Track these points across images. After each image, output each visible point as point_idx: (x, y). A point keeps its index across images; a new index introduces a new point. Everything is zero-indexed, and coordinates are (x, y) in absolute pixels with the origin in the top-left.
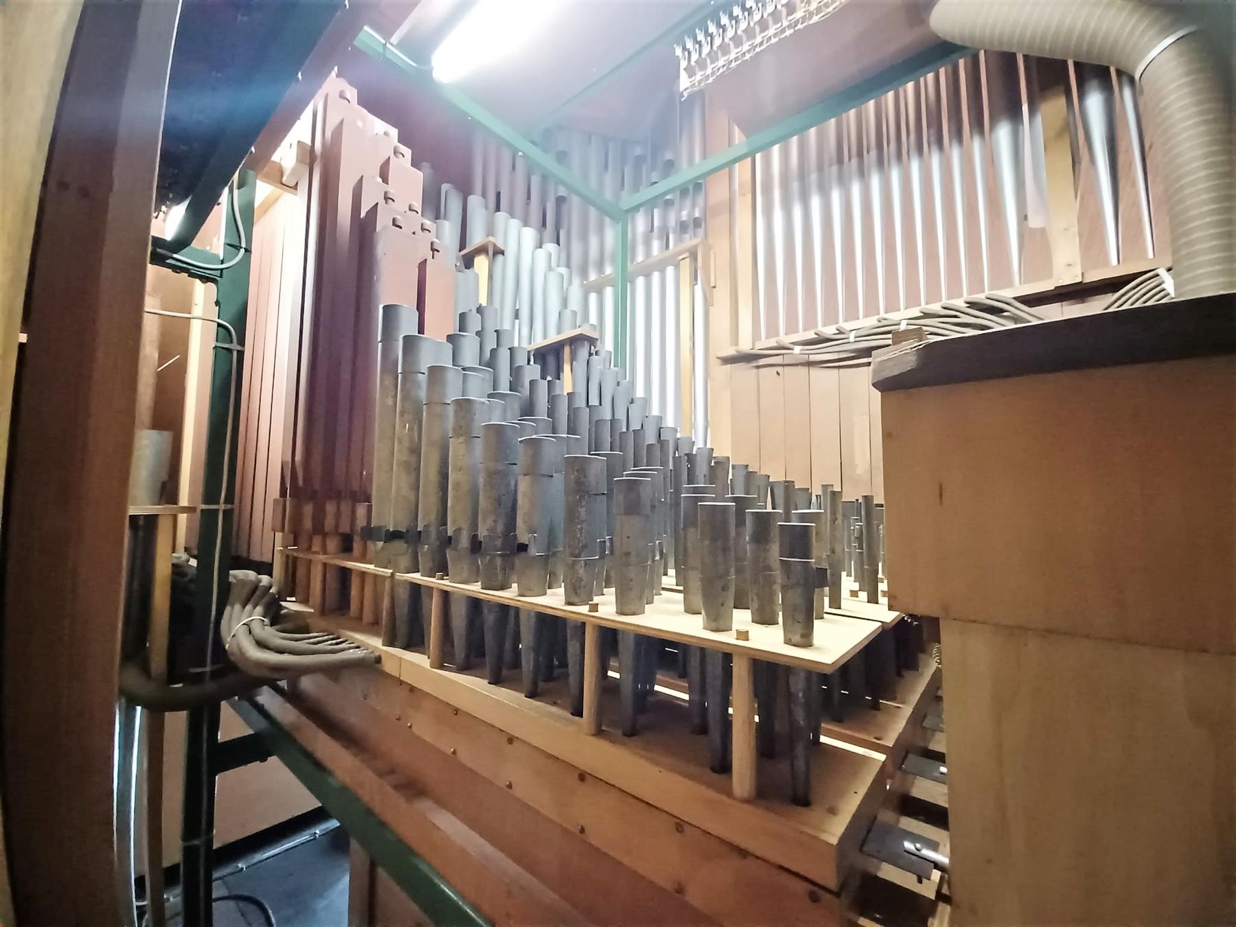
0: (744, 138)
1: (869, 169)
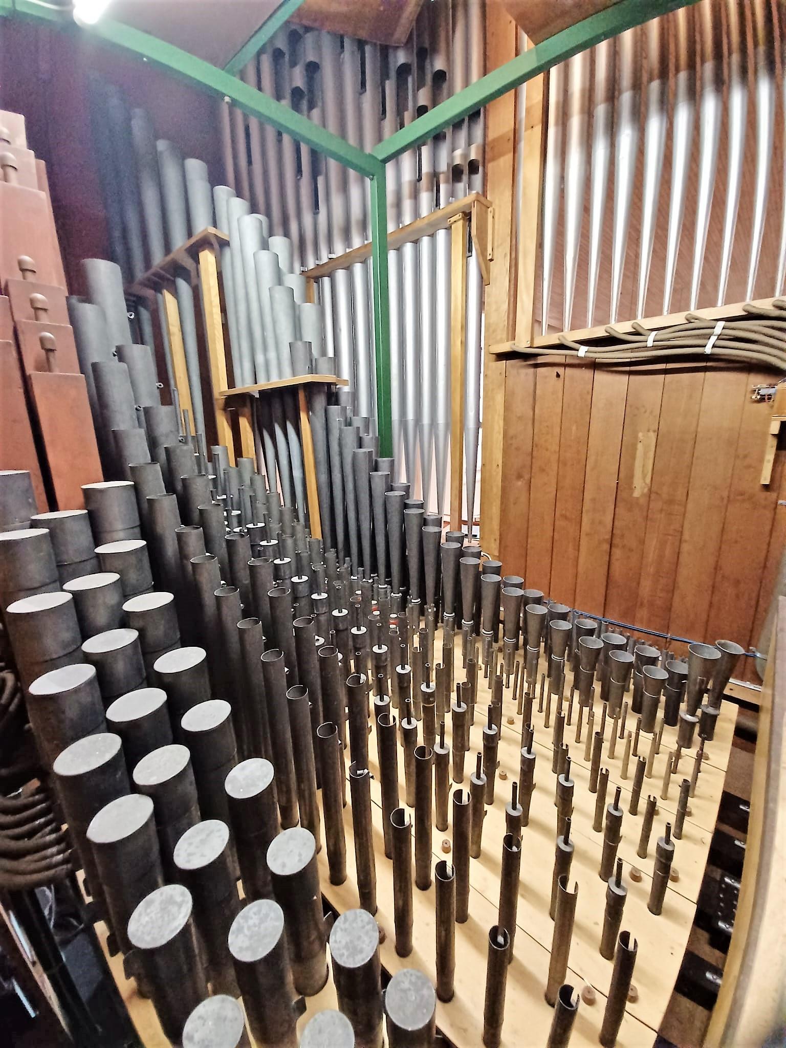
0: (532, 45)
1: (702, 88)
